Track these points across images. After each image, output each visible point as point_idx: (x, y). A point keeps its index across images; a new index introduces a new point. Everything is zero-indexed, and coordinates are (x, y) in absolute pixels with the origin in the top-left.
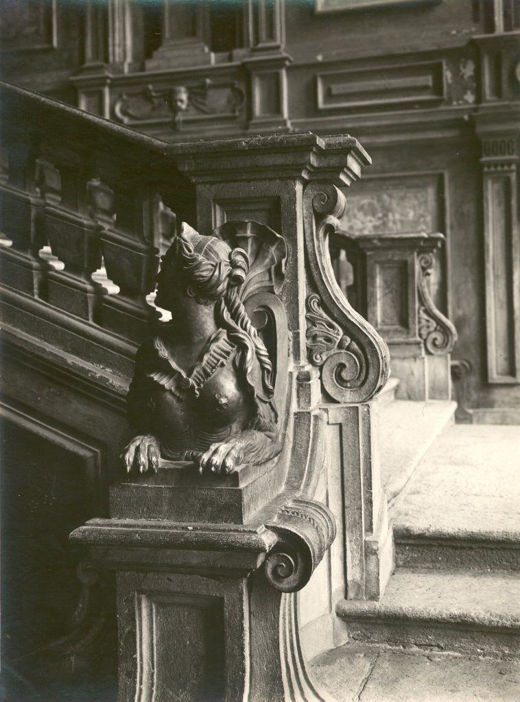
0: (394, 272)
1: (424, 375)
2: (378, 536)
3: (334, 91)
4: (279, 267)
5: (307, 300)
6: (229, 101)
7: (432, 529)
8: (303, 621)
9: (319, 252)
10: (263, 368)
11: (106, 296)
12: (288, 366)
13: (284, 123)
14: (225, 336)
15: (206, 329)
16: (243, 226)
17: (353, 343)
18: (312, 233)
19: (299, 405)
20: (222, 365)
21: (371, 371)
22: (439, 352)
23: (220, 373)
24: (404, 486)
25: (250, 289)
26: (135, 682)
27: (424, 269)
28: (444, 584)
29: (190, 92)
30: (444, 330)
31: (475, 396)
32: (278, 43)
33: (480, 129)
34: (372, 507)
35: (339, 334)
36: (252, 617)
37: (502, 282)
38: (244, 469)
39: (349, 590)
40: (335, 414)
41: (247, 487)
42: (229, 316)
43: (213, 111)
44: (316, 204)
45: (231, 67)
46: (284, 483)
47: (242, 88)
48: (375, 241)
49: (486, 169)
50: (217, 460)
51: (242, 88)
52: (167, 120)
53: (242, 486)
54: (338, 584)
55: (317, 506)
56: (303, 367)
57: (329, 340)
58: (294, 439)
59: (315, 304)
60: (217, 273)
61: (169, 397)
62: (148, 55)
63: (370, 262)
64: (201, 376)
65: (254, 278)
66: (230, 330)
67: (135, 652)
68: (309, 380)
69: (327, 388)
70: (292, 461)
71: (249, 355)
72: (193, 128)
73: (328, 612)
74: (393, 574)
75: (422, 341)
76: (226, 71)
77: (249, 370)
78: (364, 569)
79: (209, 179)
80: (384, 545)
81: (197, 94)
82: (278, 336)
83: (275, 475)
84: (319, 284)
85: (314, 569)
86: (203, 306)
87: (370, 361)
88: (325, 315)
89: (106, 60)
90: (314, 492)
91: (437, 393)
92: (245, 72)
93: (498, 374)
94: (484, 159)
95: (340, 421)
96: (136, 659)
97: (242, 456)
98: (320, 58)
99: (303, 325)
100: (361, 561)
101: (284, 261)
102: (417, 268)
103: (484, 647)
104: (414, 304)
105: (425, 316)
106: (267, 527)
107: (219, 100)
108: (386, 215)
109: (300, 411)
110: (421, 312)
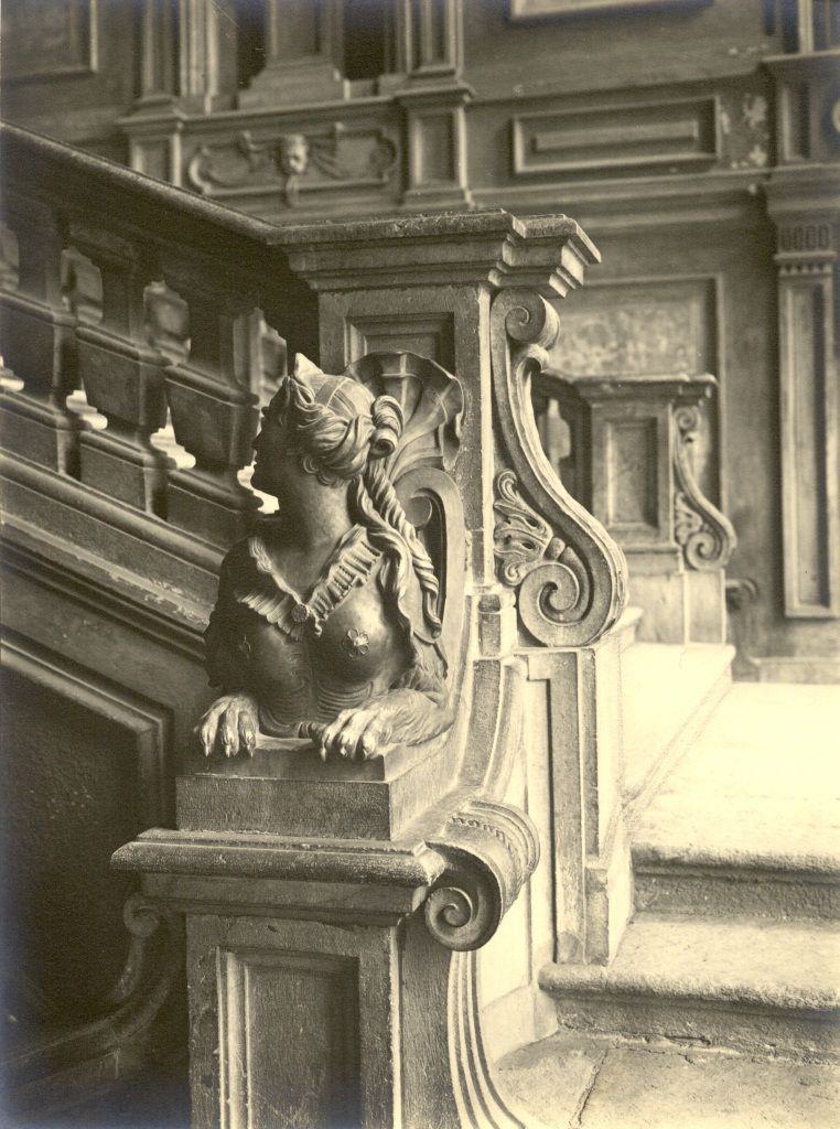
0: (634, 437)
3: (542, 144)
4: (450, 428)
6: (373, 159)
10: (424, 590)
12: (463, 586)
13: (461, 195)
17: (570, 550)
18: (504, 373)
19: (481, 650)
20: (359, 584)
21: (597, 596)
22: (708, 566)
23: (355, 597)
27: (683, 432)
29: (313, 146)
32: (452, 66)
33: (775, 207)
35: (546, 535)
36: (405, 991)
37: (809, 455)
40: (540, 663)
41: (397, 780)
42: (371, 505)
43: (346, 175)
45: (379, 104)
47: (395, 138)
48: (606, 387)
49: (783, 272)
50: (350, 737)
51: (395, 138)
53: (389, 779)
55: (511, 812)
57: (530, 545)
59: (509, 486)
60: (351, 435)
61: (274, 635)
62: (245, 84)
63: (596, 419)
66: (372, 527)
68: (498, 609)
69: (527, 623)
70: (470, 740)
72: (315, 201)
74: (631, 922)
75: (680, 548)
78: (585, 916)
79: (338, 284)
81: (322, 147)
84: (514, 454)
86: (328, 489)
87: (596, 580)
88: (524, 505)
89: (177, 92)
91: (703, 631)
92: (399, 113)
93: (801, 601)
94: (782, 255)
95: (547, 675)
96: (218, 1056)
97: (389, 730)
99: (489, 520)
100: (579, 900)
101: (458, 418)
104: (667, 487)
105: (684, 508)
107: (356, 155)
108: (622, 345)
109: (486, 658)
110: (679, 501)
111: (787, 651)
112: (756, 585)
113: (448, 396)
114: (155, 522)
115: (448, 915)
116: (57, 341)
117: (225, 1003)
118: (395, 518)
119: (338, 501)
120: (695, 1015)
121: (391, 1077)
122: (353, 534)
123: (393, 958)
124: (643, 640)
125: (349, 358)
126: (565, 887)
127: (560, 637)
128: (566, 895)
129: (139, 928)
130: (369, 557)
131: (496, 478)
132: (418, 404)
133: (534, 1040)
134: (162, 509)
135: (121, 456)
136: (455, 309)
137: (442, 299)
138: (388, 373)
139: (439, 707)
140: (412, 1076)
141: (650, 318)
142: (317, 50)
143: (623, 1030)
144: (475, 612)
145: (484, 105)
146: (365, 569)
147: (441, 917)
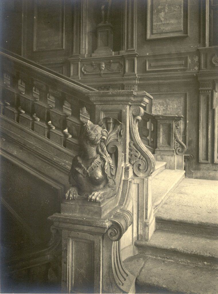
1: (175, 161)
2: (149, 220)
3: (152, 65)
4: (120, 133)
5: (129, 143)
6: (118, 68)
7: (168, 218)
8: (121, 248)
9: (134, 127)
10: (111, 168)
11: (68, 139)
12: (122, 165)
14: (99, 157)
15: (93, 154)
16: (110, 119)
17: (144, 158)
18: (132, 122)
19: (125, 178)
20: (98, 166)
21: (149, 167)
23: (97, 169)
24: (159, 205)
25: (111, 140)
26: (67, 265)
27: (176, 126)
28: (171, 237)
30: (182, 147)
31: (194, 167)
32: (134, 49)
33: (199, 79)
34: (147, 211)
35: (139, 155)
36: (103, 248)
37: (205, 130)
38: (103, 200)
39: (139, 237)
40: (136, 181)
41: (103, 206)
42: (101, 151)
44: (133, 113)
45: (119, 56)
46: (118, 203)
49: (201, 92)
50: (94, 198)
52: (99, 73)
53: (102, 206)
54: (135, 235)
55: (128, 212)
56: (127, 165)
57: (136, 156)
58: (123, 188)
59: (132, 144)
60: (97, 137)
61: (81, 176)
62: (93, 52)
63: (158, 124)
64: (91, 169)
65: (113, 135)
66: (101, 155)
67: (67, 256)
68: (128, 169)
69: (135, 172)
70: (121, 196)
71: (106, 164)
73: (132, 244)
74: (155, 232)
75: (175, 150)
76: (118, 58)
77: (106, 169)
78: (144, 231)
79: (99, 103)
80: (151, 223)
81: (108, 65)
82: (119, 155)
83: (115, 201)
84: (133, 138)
85: (123, 233)
86: (93, 147)
87: (149, 164)
88: (135, 148)
89: (80, 53)
90: (128, 206)
91: (179, 167)
92: (123, 58)
93: (202, 159)
94: (200, 89)
95: (138, 182)
96: (67, 258)
97: (102, 196)
98: (148, 54)
99: (128, 151)
100: (143, 228)
101: (122, 131)
102: (174, 126)
103: (181, 259)
104: (173, 138)
105: (176, 142)
106: (109, 220)
108: (167, 106)
109: (126, 179)
110: (175, 141)
111: (198, 169)
112: (193, 156)
113: (120, 127)
114: (64, 148)
115: (112, 234)
116: (46, 111)
117: (69, 248)
118: (106, 153)
119: (94, 150)
120: (165, 252)
121: (100, 265)
122: (97, 156)
123: (101, 242)
124: (166, 169)
125: (101, 118)
126: (140, 225)
127: (141, 175)
128: (140, 227)
129: (53, 232)
130: (100, 161)
131: (130, 142)
132: (114, 128)
133: (133, 255)
134: (65, 146)
135: (57, 135)
136: (122, 109)
137: (120, 107)
138: (108, 122)
139: (113, 191)
140: (104, 265)
141: (174, 100)
142: (108, 45)
143: (151, 255)
144: (124, 170)
145: (141, 57)
146: (99, 163)
147: (110, 234)
